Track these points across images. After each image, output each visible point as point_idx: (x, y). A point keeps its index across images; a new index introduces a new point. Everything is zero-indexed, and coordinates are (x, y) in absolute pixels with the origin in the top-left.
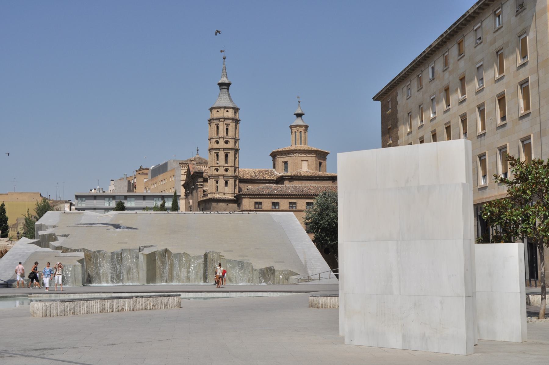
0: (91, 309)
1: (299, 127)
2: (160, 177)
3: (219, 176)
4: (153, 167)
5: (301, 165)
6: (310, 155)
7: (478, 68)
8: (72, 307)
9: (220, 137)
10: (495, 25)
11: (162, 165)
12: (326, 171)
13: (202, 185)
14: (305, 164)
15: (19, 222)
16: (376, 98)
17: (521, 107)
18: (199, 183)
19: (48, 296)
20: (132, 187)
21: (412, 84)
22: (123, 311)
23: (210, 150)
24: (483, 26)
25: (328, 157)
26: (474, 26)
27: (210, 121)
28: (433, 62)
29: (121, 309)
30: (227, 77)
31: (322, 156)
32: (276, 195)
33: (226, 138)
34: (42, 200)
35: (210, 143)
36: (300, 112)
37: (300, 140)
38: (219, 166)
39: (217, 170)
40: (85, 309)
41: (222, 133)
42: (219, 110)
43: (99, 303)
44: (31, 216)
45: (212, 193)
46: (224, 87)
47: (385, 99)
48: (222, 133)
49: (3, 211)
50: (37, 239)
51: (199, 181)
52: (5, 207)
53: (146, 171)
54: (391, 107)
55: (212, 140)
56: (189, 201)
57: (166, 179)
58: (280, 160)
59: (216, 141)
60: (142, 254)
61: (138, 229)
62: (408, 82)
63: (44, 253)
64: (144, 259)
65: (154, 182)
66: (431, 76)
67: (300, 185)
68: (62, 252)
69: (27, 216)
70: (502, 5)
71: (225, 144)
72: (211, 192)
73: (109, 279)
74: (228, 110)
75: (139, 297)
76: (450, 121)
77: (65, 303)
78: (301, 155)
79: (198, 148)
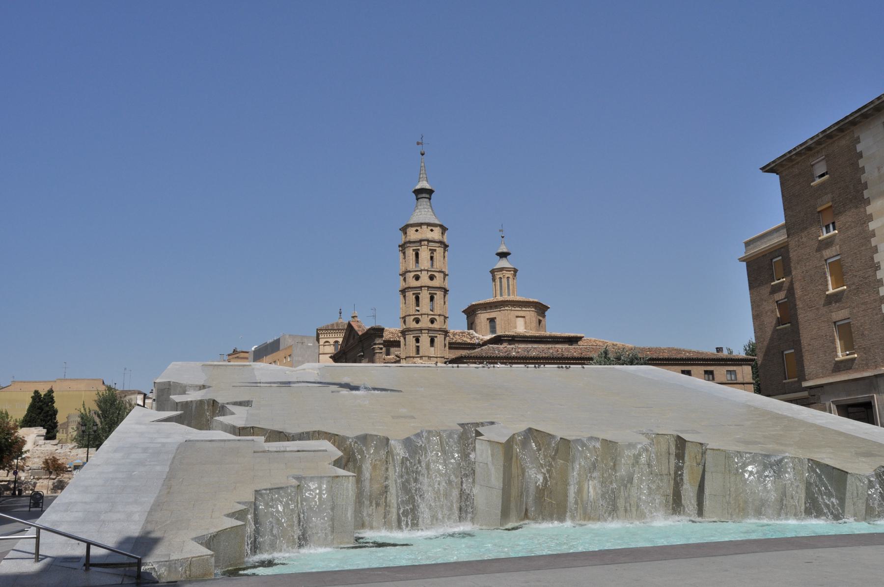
1: (507, 271)
3: (421, 330)
4: (255, 347)
6: (527, 309)
9: (423, 268)
11: (270, 343)
12: (545, 332)
15: (72, 419)
18: (377, 346)
23: (403, 291)
31: (541, 309)
33: (431, 271)
37: (500, 291)
41: (425, 262)
42: (418, 228)
44: (90, 411)
45: (410, 357)
46: (424, 195)
47: (798, 163)
48: (425, 262)
49: (51, 400)
51: (377, 342)
57: (277, 361)
58: (482, 318)
59: (415, 275)
61: (401, 391)
71: (430, 281)
72: (408, 356)
73: (394, 517)
74: (433, 228)
78: (515, 309)
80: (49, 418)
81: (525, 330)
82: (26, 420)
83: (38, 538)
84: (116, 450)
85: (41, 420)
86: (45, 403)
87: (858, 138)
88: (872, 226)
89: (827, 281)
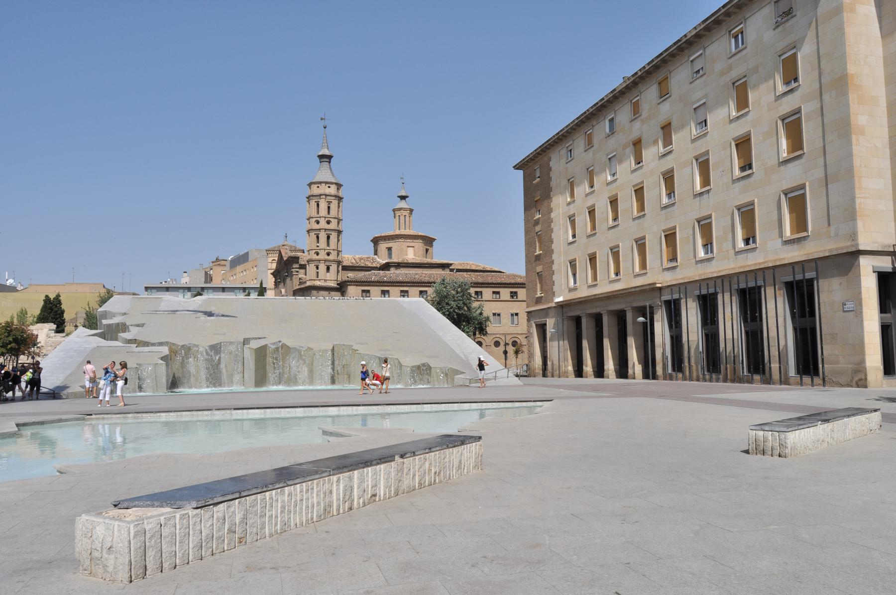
0: (295, 512)
1: (404, 210)
2: (239, 268)
4: (231, 257)
5: (407, 251)
6: (417, 241)
7: (695, 109)
8: (238, 518)
9: (321, 215)
10: (731, 48)
11: (242, 255)
12: (432, 259)
13: (297, 272)
14: (411, 250)
16: (517, 167)
17: (783, 148)
19: (121, 418)
20: (208, 278)
21: (575, 144)
22: (375, 501)
23: (308, 231)
24: (706, 53)
25: (434, 243)
26: (690, 56)
27: (309, 198)
28: (613, 112)
29: (369, 496)
30: (328, 149)
31: (428, 241)
32: (386, 282)
34: (106, 292)
35: (309, 223)
36: (404, 194)
38: (320, 249)
39: (318, 254)
40: (276, 517)
41: (323, 211)
42: (319, 185)
43: (315, 490)
44: (93, 310)
45: (312, 280)
46: (325, 160)
47: (530, 166)
48: (323, 211)
50: (100, 330)
52: (61, 298)
53: (223, 263)
54: (540, 174)
55: (311, 219)
56: (281, 291)
58: (383, 246)
60: (249, 348)
61: (237, 317)
62: (568, 142)
63: (110, 348)
64: (251, 354)
65: (233, 273)
66: (607, 130)
67: (406, 272)
68: (137, 347)
69: (88, 309)
70: (745, 20)
75: (407, 456)
76: (643, 181)
77: (216, 509)
80: (58, 316)
81: (414, 257)
82: (40, 318)
85: (52, 318)
86: (54, 305)
89: (536, 246)
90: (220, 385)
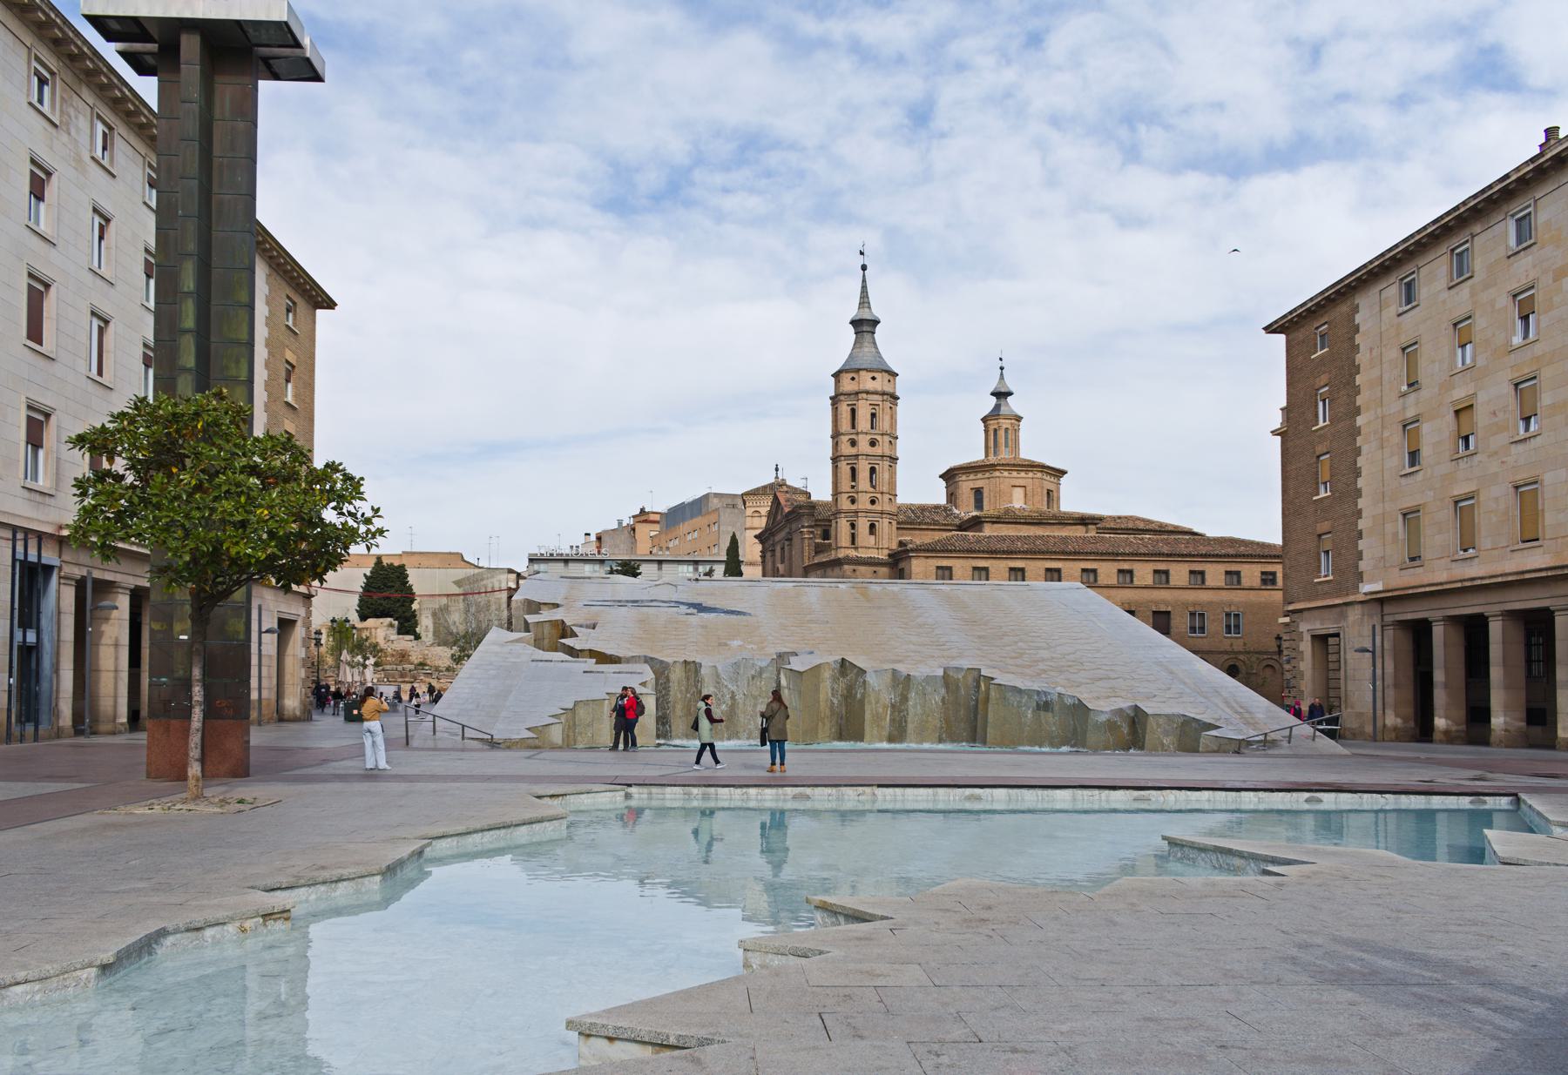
74: (876, 375)
79: (1001, 395)
83: (434, 721)
84: (494, 644)
87: (1358, 306)
88: (1360, 421)
90: (862, 740)
